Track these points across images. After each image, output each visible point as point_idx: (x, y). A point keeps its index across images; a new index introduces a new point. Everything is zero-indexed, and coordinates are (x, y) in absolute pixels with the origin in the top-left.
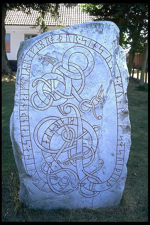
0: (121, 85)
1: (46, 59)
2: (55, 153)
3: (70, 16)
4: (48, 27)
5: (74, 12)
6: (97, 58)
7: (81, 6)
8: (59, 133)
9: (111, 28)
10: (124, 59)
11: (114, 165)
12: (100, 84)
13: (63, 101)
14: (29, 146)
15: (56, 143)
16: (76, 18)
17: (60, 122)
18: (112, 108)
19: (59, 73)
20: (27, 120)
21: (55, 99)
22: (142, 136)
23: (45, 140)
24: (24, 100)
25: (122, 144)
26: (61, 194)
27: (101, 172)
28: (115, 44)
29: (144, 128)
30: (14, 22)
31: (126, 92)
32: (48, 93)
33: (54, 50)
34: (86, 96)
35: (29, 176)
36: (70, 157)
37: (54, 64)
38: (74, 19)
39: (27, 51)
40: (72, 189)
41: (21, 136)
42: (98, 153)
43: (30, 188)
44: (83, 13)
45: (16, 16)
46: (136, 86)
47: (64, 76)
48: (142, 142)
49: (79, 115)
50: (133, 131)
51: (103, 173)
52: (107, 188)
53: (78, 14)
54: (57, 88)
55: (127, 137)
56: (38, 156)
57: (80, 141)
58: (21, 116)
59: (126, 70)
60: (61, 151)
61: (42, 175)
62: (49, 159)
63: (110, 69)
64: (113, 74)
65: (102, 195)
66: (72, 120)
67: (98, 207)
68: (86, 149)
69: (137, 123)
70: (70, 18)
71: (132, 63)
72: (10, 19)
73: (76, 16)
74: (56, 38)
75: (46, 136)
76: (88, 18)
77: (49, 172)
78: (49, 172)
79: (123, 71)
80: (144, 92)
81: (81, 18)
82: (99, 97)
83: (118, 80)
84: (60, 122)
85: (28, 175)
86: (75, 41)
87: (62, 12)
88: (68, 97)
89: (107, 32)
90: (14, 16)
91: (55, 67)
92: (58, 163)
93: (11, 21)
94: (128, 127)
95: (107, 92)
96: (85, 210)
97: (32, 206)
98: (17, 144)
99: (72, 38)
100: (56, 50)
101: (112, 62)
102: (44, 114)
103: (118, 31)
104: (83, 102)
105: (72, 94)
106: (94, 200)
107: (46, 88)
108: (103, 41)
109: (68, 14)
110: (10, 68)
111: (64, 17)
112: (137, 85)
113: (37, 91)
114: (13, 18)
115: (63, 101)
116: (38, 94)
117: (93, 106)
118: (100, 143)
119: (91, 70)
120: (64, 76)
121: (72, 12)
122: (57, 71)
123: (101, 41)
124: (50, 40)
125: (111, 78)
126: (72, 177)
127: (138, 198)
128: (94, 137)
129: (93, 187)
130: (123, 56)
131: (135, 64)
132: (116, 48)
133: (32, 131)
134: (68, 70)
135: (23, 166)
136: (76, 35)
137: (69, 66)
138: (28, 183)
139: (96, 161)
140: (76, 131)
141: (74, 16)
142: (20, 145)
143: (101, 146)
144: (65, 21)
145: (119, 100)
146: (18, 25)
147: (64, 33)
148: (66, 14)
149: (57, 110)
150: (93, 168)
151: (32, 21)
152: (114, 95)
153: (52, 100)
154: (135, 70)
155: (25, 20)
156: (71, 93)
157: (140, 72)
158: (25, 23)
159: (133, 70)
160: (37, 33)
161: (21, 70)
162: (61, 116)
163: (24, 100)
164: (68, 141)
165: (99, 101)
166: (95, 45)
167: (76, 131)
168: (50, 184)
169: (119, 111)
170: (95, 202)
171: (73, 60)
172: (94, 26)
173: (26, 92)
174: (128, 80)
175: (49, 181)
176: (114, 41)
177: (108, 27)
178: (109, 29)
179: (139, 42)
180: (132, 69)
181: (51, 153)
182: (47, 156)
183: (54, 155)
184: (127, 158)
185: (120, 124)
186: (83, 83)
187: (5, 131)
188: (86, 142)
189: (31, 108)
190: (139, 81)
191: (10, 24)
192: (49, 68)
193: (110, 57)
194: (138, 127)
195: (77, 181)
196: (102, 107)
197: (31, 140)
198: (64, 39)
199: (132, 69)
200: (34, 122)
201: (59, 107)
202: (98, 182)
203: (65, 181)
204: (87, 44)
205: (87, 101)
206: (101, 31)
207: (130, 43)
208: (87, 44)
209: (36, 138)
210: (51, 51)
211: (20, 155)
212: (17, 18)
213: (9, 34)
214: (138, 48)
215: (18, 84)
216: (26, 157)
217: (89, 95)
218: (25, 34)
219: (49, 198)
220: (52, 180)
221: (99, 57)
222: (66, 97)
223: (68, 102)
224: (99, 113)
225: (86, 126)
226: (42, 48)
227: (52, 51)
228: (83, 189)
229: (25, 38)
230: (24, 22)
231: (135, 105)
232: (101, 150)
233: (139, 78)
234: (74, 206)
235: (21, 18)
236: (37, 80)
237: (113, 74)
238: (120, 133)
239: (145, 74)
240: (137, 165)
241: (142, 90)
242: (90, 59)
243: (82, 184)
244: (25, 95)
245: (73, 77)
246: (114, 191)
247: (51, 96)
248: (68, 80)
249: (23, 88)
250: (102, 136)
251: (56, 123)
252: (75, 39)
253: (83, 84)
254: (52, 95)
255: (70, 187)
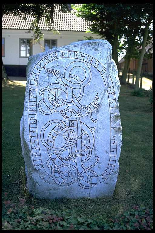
0: (113, 94)
1: (51, 72)
2: (58, 151)
3: (65, 20)
4: (42, 32)
5: (70, 17)
6: (94, 71)
7: (77, 7)
8: (61, 133)
9: (105, 46)
10: (116, 72)
11: (107, 162)
12: (96, 93)
13: (65, 107)
14: (37, 145)
15: (59, 142)
16: (72, 22)
17: (62, 124)
18: (106, 113)
19: (62, 83)
20: (35, 123)
21: (59, 106)
22: (135, 139)
23: (50, 139)
24: (33, 106)
25: (114, 143)
26: (64, 186)
27: (97, 166)
28: (109, 59)
29: (137, 132)
30: (8, 25)
31: (118, 99)
32: (53, 100)
33: (57, 64)
34: (85, 102)
35: (37, 171)
36: (71, 154)
37: (58, 76)
38: (70, 24)
39: (35, 65)
40: (73, 181)
41: (30, 136)
42: (95, 151)
43: (38, 181)
44: (78, 18)
45: (11, 20)
46: (132, 91)
47: (66, 86)
48: (134, 144)
49: (78, 119)
50: (124, 133)
51: (99, 167)
52: (102, 180)
53: (74, 19)
54: (60, 96)
55: (119, 137)
56: (44, 153)
57: (79, 141)
58: (30, 119)
59: (118, 81)
60: (63, 149)
61: (47, 170)
62: (53, 156)
63: (104, 80)
64: (107, 85)
65: (98, 186)
66: (73, 122)
67: (94, 197)
68: (84, 148)
69: (130, 127)
70: (65, 22)
71: (127, 68)
72: (5, 23)
73: (72, 20)
74: (59, 54)
75: (51, 136)
76: (84, 25)
77: (53, 167)
78: (53, 167)
79: (115, 81)
80: (139, 98)
81: (76, 22)
82: (95, 104)
83: (111, 90)
84: (62, 124)
85: (36, 170)
86: (76, 57)
87: (57, 16)
88: (69, 104)
89: (102, 50)
90: (8, 20)
91: (59, 79)
92: (61, 159)
93: (6, 25)
94: (119, 128)
95: (102, 99)
96: (83, 199)
97: (39, 196)
98: (26, 143)
99: (73, 54)
100: (60, 64)
101: (106, 74)
102: (49, 118)
103: (111, 48)
104: (82, 108)
105: (72, 101)
106: (91, 191)
107: (51, 96)
108: (99, 57)
109: (64, 18)
110: (6, 73)
111: (59, 21)
112: (133, 90)
113: (43, 99)
114: (8, 22)
115: (65, 107)
116: (45, 101)
117: (90, 111)
118: (96, 142)
119: (88, 81)
120: (66, 86)
121: (68, 17)
122: (61, 82)
123: (97, 57)
124: (55, 56)
125: (105, 88)
126: (73, 172)
127: (129, 190)
128: (91, 137)
129: (91, 180)
130: (115, 69)
131: (131, 69)
132: (109, 62)
133: (39, 132)
134: (70, 81)
135: (31, 162)
136: (76, 52)
137: (70, 77)
138: (36, 176)
139: (93, 158)
140: (76, 132)
141: (70, 20)
142: (29, 144)
143: (97, 145)
144: (61, 25)
145: (112, 106)
146: (13, 29)
147: (66, 50)
148: (61, 18)
149: (60, 115)
150: (90, 164)
151: (27, 25)
152: (107, 102)
153: (56, 106)
154: (130, 74)
155: (20, 24)
156: (72, 100)
157: (135, 77)
158: (20, 27)
159: (129, 74)
160: (31, 38)
161: (30, 80)
162: (64, 120)
163: (33, 106)
164: (70, 140)
165: (95, 107)
166: (91, 60)
167: (76, 132)
168: (54, 177)
169: (112, 115)
170: (92, 193)
171: (74, 72)
172: (91, 45)
173: (34, 99)
174: (119, 90)
175: (53, 175)
176: (108, 57)
177: (103, 45)
178: (103, 47)
179: (134, 47)
180: (128, 74)
181: (55, 151)
182: (52, 153)
183: (58, 152)
184: (119, 155)
185: (113, 126)
186: (82, 92)
187: (7, 134)
188: (84, 141)
189: (38, 113)
190: (134, 86)
191: (5, 27)
192: (53, 80)
193: (104, 71)
194: (132, 131)
195: (77, 174)
196: (98, 112)
197: (38, 140)
198: (66, 56)
199: (128, 74)
200: (41, 125)
201: (61, 111)
202: (94, 175)
203: (66, 174)
204: (85, 60)
205: (85, 107)
206: (97, 48)
207: (125, 49)
208: (85, 60)
209: (42, 138)
210: (55, 65)
211: (28, 153)
212: (12, 22)
213: (4, 38)
214: (133, 53)
215: (27, 92)
216: (34, 154)
217: (87, 102)
218: (20, 39)
219: (53, 189)
220: (55, 174)
221: (96, 70)
222: (68, 104)
223: (69, 108)
224: (95, 117)
225: (84, 127)
226: (47, 62)
227: (56, 65)
228: (81, 181)
229: (20, 41)
230: (19, 26)
231: (130, 110)
232: (97, 149)
233: (134, 83)
234: (75, 196)
235: (16, 22)
236: (44, 89)
237: (107, 85)
238: (113, 134)
239: (140, 79)
240: (129, 164)
241: (137, 96)
242: (88, 72)
243: (81, 177)
244: (33, 102)
245: (73, 87)
246: (108, 183)
247: (55, 103)
248: (69, 89)
249: (32, 95)
250: (97, 136)
251: (59, 125)
252: (75, 55)
253: (82, 93)
254: (56, 102)
255: (71, 180)
